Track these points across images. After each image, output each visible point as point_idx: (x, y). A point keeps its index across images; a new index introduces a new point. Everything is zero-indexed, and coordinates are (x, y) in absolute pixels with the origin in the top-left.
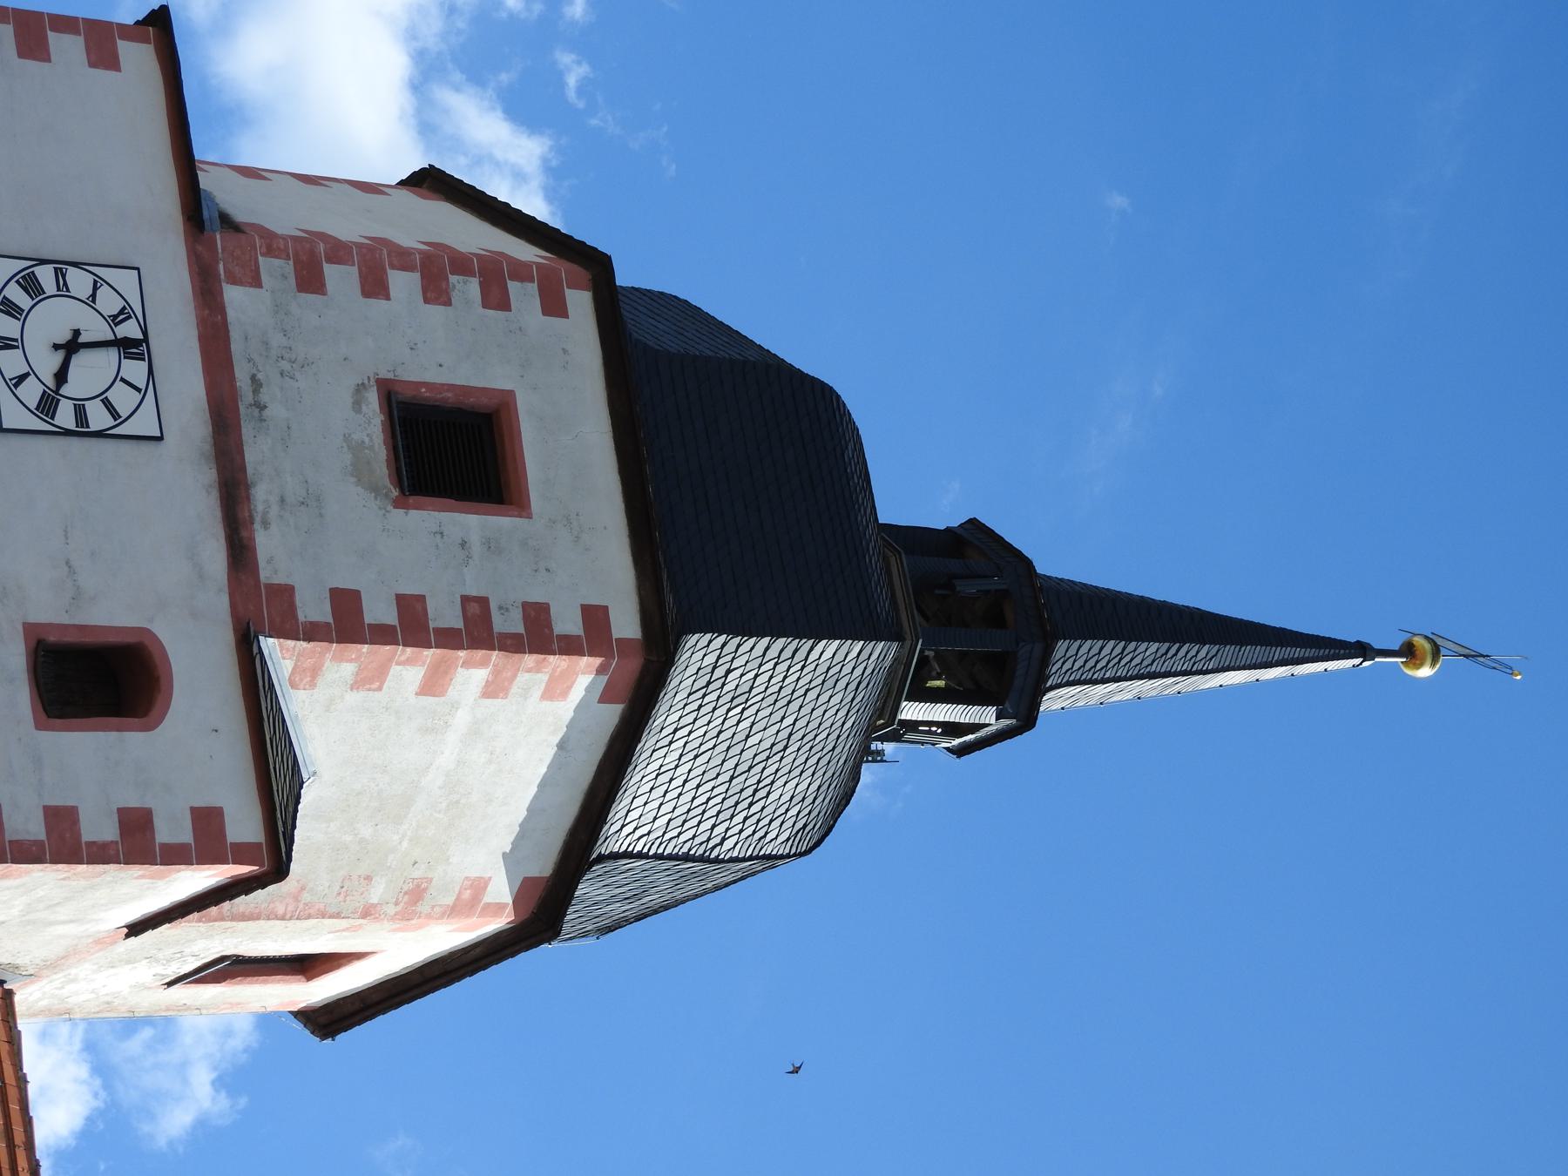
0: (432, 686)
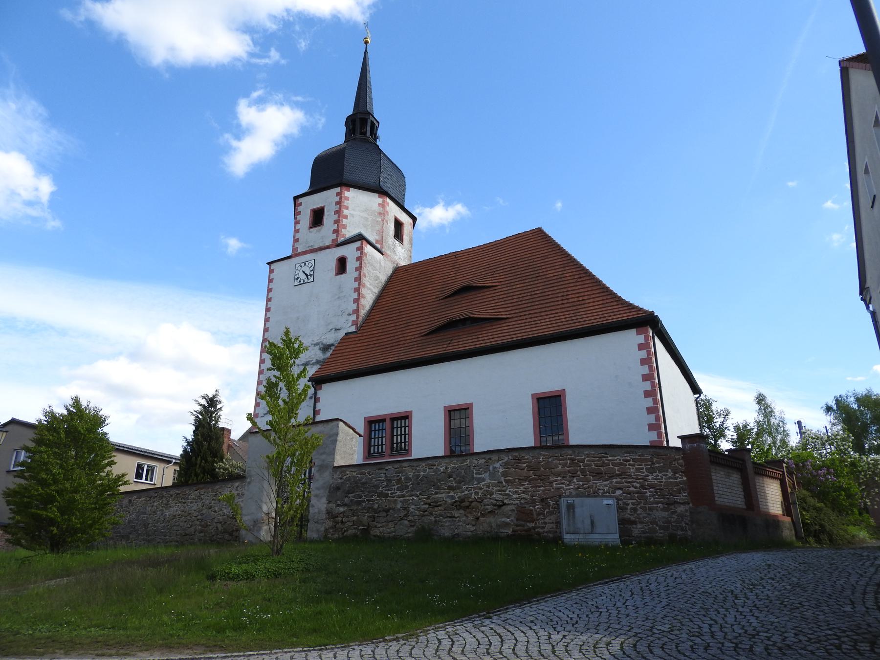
0: (346, 217)
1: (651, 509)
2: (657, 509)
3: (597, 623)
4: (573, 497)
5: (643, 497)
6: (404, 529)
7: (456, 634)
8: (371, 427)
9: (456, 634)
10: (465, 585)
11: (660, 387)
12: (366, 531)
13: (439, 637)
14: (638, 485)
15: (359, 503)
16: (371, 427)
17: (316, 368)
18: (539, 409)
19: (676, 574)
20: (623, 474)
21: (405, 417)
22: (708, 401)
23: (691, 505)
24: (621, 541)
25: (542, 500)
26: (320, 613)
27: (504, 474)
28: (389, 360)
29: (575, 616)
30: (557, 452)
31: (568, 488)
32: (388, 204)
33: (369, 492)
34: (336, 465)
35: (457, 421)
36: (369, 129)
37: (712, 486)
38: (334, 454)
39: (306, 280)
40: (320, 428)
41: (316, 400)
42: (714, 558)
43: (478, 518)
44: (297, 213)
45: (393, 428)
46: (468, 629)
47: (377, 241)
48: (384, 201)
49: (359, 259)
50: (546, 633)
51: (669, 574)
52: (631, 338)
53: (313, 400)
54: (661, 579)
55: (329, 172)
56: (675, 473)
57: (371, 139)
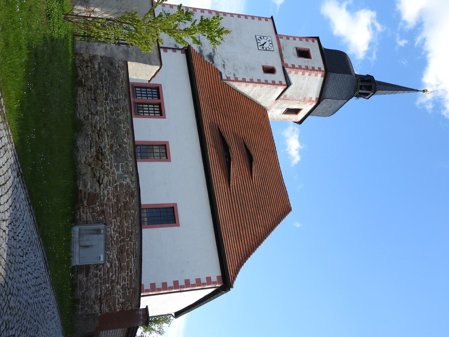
0: (303, 74)
1: (96, 287)
2: (97, 291)
3: (14, 254)
4: (106, 233)
5: (105, 281)
6: (82, 112)
7: (6, 151)
8: (154, 88)
9: (6, 151)
10: (42, 157)
11: (181, 291)
12: (80, 84)
13: (3, 139)
14: (113, 278)
15: (101, 79)
16: (154, 88)
17: (197, 50)
18: (166, 208)
19: (51, 307)
20: (121, 268)
21: (161, 113)
22: (169, 321)
23: (99, 314)
24: (74, 267)
25: (103, 212)
26: (21, 49)
27: (121, 185)
28: (202, 103)
29: (20, 238)
30: (137, 222)
31: (112, 231)
32: (311, 104)
33: (109, 87)
34: (129, 63)
35: (158, 151)
36: (364, 92)
37: (113, 329)
38: (136, 62)
39: (259, 44)
40: (156, 52)
41: (174, 50)
42: (62, 332)
43: (90, 165)
44: (307, 38)
45: (154, 104)
46: (9, 160)
47: (285, 96)
48: (313, 101)
49: (273, 83)
50: (7, 218)
51: (51, 303)
52: (215, 272)
53: (174, 47)
54: (47, 297)
55: (335, 62)
56: (122, 304)
57: (357, 93)
